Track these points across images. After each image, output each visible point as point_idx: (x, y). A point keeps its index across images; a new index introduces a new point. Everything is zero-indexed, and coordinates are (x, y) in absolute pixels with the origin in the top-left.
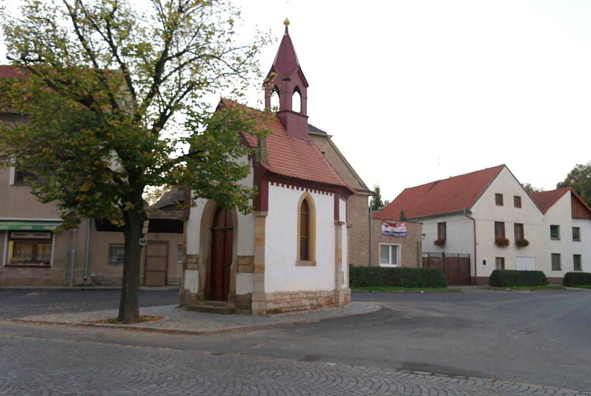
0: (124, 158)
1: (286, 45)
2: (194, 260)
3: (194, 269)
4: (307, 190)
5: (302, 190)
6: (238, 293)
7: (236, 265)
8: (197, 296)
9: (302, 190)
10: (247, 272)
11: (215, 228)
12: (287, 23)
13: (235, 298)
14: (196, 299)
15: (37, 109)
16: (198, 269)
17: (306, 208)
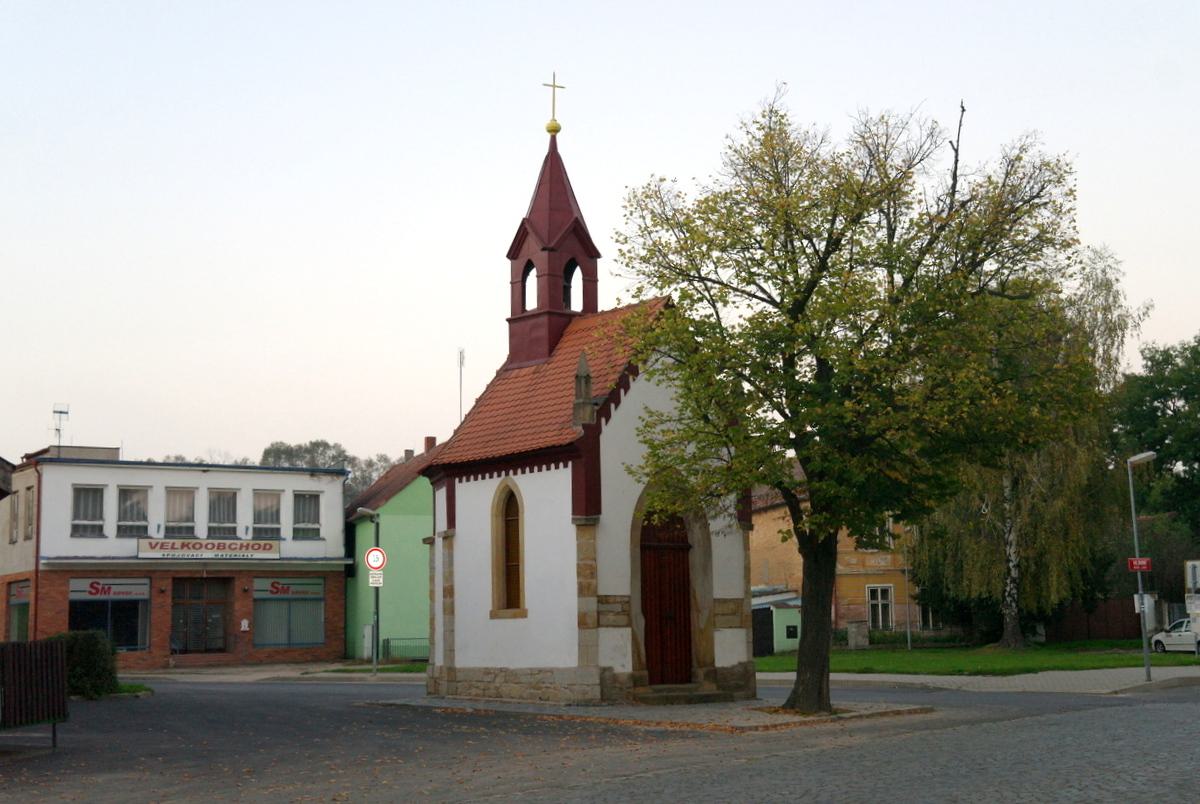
0: (769, 339)
1: (554, 173)
2: (618, 608)
4: (507, 474)
5: (499, 476)
6: (719, 664)
7: (634, 622)
8: (635, 680)
9: (499, 476)
11: (510, 564)
12: (554, 130)
13: (714, 674)
14: (632, 684)
15: (773, 251)
16: (629, 625)
17: (509, 509)
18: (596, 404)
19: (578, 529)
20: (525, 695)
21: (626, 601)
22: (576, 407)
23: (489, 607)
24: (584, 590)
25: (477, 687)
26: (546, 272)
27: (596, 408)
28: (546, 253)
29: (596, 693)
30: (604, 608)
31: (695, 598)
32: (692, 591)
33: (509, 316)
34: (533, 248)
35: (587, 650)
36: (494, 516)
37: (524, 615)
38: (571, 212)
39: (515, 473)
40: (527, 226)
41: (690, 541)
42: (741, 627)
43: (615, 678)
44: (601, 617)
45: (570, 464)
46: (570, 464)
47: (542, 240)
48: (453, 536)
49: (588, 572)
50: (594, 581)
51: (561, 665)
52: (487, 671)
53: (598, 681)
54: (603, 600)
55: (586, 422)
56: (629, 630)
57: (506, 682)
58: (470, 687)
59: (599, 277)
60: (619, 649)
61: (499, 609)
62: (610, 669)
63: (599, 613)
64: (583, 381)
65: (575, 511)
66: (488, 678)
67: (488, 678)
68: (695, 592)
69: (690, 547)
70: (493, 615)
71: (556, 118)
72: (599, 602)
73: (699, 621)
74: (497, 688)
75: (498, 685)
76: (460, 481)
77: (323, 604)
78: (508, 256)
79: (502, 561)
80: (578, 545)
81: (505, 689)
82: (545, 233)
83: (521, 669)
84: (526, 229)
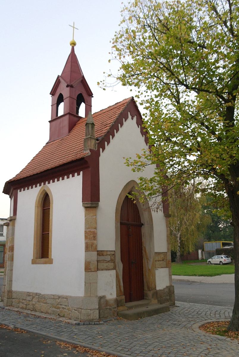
1: (73, 61)
2: (108, 258)
3: (108, 269)
5: (40, 185)
6: (158, 289)
8: (118, 303)
9: (40, 185)
10: (162, 268)
12: (73, 44)
13: (157, 294)
16: (114, 268)
17: (45, 201)
18: (97, 140)
19: (86, 210)
20: (49, 311)
21: (165, 254)
22: (86, 140)
23: (31, 257)
24: (89, 247)
25: (22, 303)
26: (69, 96)
27: (97, 142)
28: (68, 89)
29: (96, 315)
30: (101, 258)
31: (145, 252)
32: (143, 249)
33: (50, 119)
34: (65, 91)
35: (90, 285)
36: (37, 207)
37: (51, 262)
38: (81, 74)
39: (49, 183)
40: (60, 78)
41: (142, 222)
42: (166, 267)
43: (107, 301)
44: (99, 264)
45: (81, 173)
46: (81, 173)
47: (67, 82)
48: (15, 219)
49: (92, 236)
50: (95, 242)
51: (73, 295)
52: (29, 294)
53: (97, 307)
54: (100, 253)
55: (92, 148)
56: (115, 271)
57: (39, 302)
58: (19, 302)
59: (92, 105)
60: (109, 285)
61: (37, 258)
62: (104, 297)
63: (98, 261)
64: (90, 126)
65: (83, 200)
66: (29, 298)
67: (29, 298)
68: (145, 248)
69: (143, 224)
70: (34, 262)
71: (74, 39)
72: (98, 254)
73: (148, 264)
74: (33, 305)
75: (34, 303)
76: (20, 191)
77: (3, 253)
78: (50, 94)
79: (40, 233)
80: (86, 220)
81: (38, 306)
82: (68, 80)
83: (48, 295)
84: (59, 80)
